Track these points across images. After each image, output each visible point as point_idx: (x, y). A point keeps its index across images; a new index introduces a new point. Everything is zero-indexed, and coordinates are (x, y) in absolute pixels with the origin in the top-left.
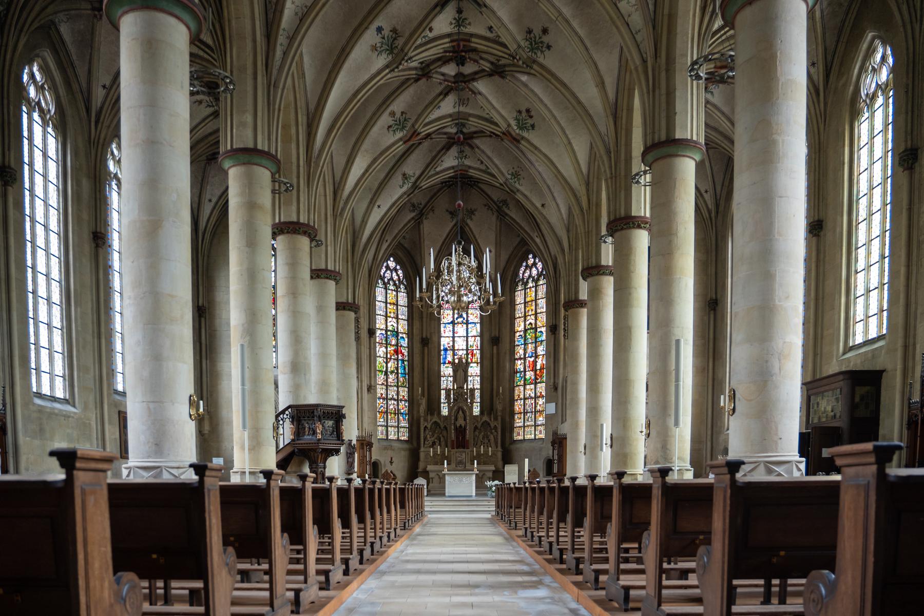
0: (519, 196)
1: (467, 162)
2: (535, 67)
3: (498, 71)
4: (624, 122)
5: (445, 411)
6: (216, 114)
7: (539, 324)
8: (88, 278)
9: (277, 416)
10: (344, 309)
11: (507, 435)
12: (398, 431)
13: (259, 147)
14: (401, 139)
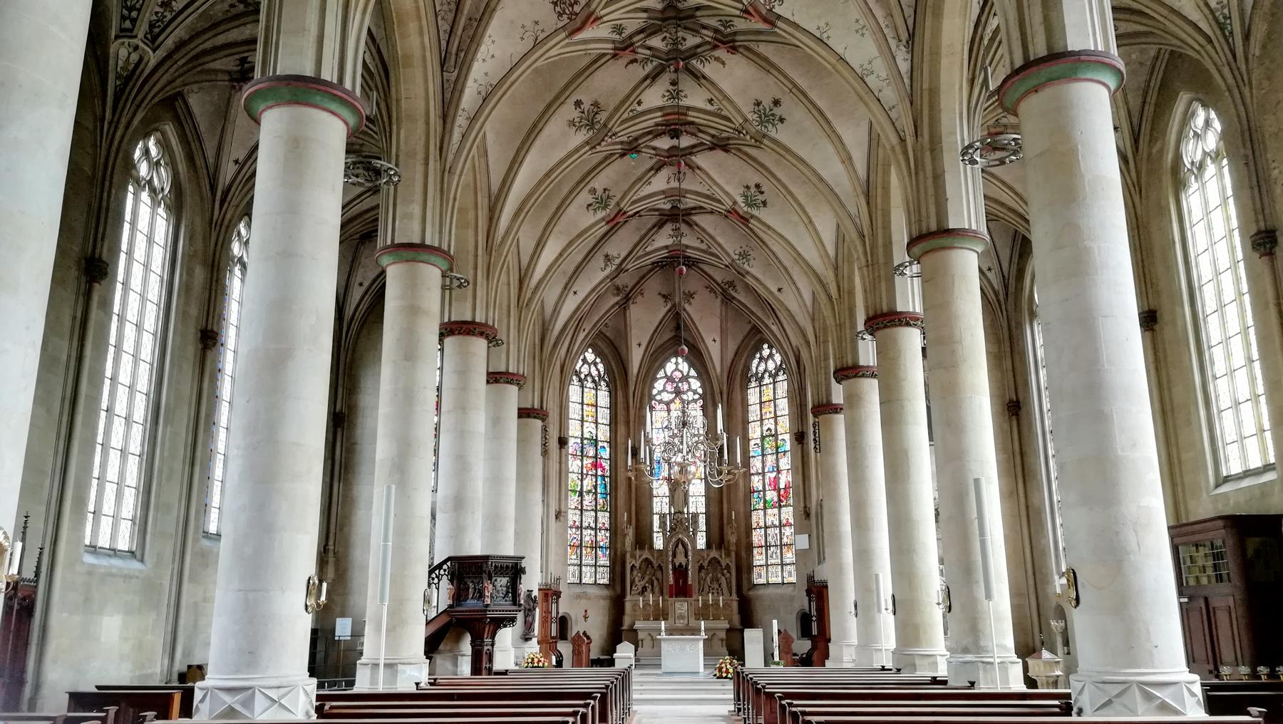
0: (749, 280)
1: (685, 241)
2: (765, 141)
3: (721, 145)
4: (879, 200)
5: (659, 543)
6: (375, 190)
7: (780, 430)
8: (188, 389)
9: (430, 572)
10: (529, 416)
11: (745, 576)
12: (597, 572)
13: (428, 242)
14: (603, 219)
